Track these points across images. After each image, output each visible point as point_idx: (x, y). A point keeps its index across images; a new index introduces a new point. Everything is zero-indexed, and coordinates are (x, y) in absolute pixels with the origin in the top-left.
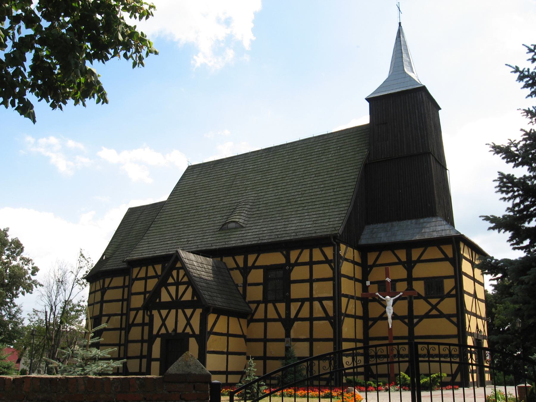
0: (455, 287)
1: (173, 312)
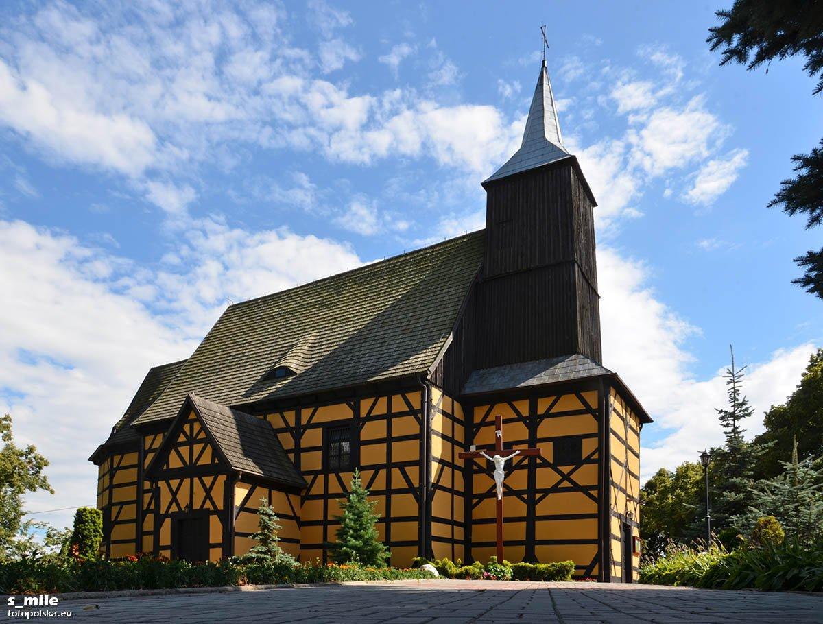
0: (599, 450)
1: (187, 481)
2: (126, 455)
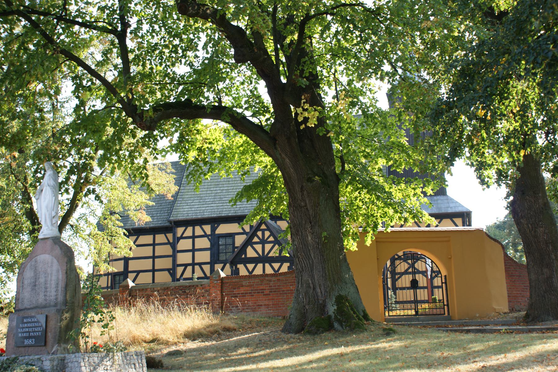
2: (141, 237)
